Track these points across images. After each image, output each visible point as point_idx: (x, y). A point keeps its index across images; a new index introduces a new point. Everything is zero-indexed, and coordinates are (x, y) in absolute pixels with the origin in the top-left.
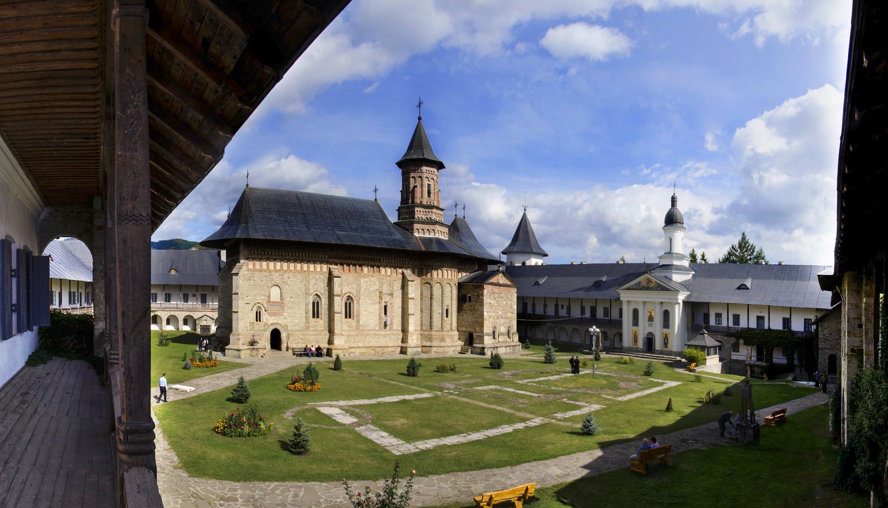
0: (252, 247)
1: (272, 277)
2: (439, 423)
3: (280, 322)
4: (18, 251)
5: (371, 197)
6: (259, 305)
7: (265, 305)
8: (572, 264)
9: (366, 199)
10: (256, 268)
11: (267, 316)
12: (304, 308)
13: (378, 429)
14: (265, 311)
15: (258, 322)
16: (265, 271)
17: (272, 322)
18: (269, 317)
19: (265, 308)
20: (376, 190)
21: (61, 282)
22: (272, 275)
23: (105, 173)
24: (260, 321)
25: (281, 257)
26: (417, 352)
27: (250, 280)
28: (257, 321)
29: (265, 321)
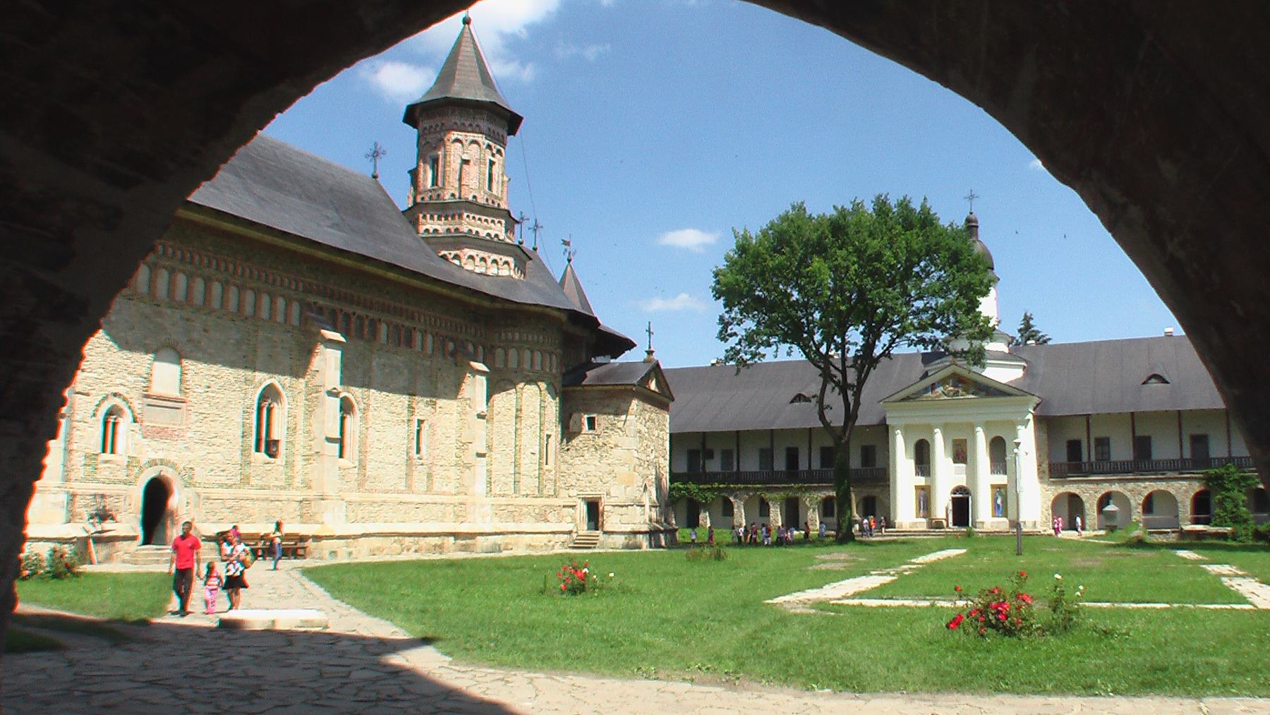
1: (159, 320)
2: (1007, 618)
3: (173, 457)
5: (364, 169)
12: (240, 420)
13: (1234, 569)
17: (153, 456)
20: (376, 154)
24: (113, 452)
25: (189, 267)
26: (495, 544)
28: (104, 451)
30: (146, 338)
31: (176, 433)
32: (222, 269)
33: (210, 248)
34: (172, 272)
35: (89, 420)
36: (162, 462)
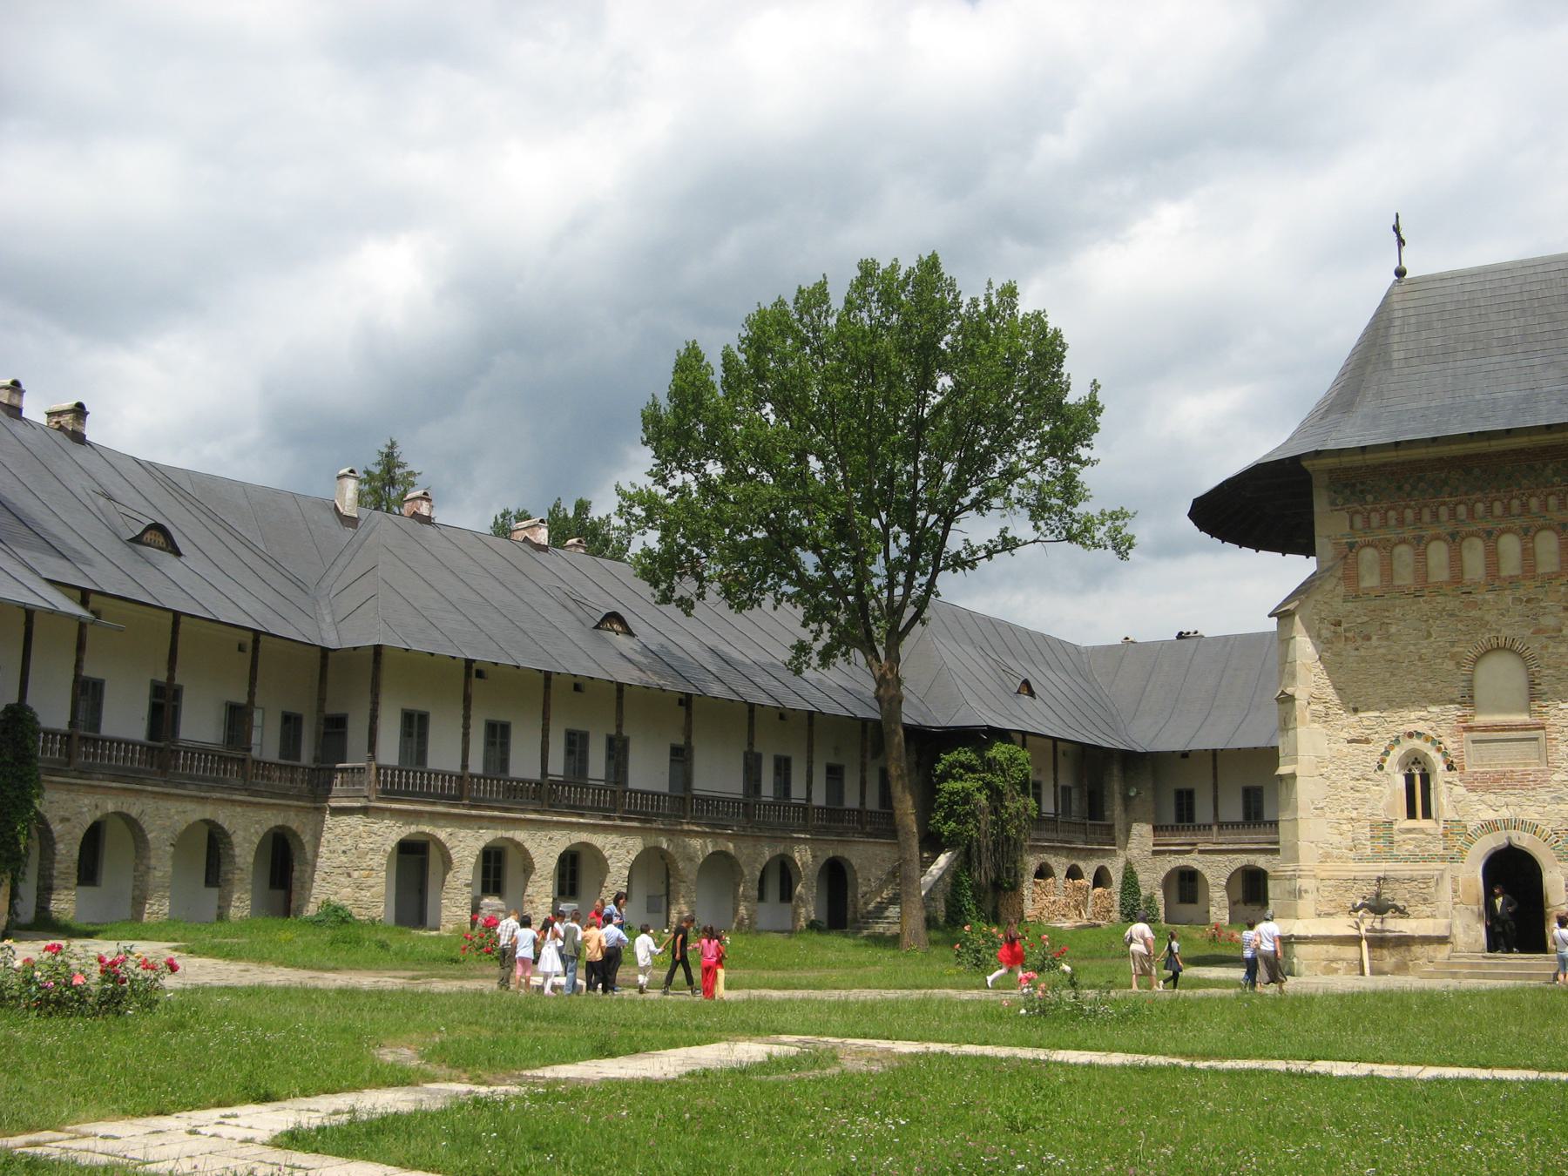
0: (1370, 498)
3: (1531, 814)
4: (280, 758)
6: (1417, 743)
7: (1448, 743)
8: (1284, 555)
9: (1530, 257)
10: (1397, 582)
11: (1460, 790)
14: (1450, 767)
15: (1420, 823)
16: (1438, 590)
17: (1490, 815)
18: (1473, 797)
19: (1445, 754)
21: (811, 724)
22: (1475, 605)
23: (105, 931)
24: (1427, 814)
27: (1368, 638)
28: (1411, 814)
29: (1449, 814)
30: (1453, 644)
31: (1531, 778)
32: (1393, 522)
33: (1557, 479)
34: (1490, 536)
35: (1372, 775)
36: (1508, 824)
